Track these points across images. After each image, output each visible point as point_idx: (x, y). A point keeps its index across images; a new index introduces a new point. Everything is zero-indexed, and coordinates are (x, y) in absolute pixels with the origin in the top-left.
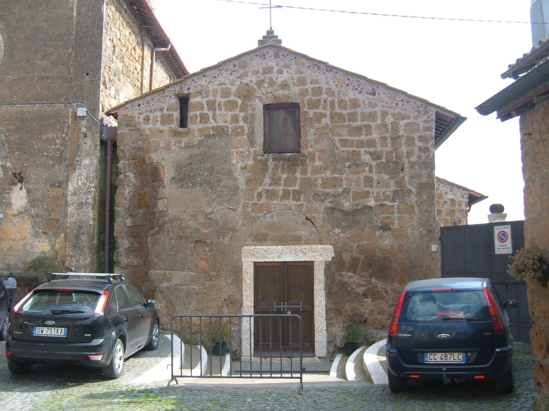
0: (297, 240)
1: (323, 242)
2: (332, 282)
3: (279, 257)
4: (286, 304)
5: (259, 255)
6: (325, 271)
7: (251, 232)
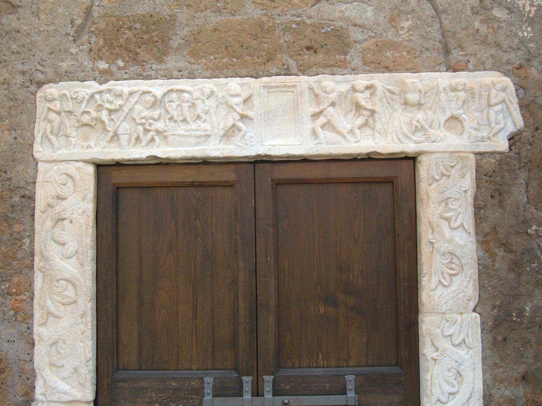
0: (321, 49)
1: (456, 55)
2: (516, 266)
3: (230, 133)
4: (268, 387)
5: (125, 127)
6: (479, 209)
7: (88, 12)
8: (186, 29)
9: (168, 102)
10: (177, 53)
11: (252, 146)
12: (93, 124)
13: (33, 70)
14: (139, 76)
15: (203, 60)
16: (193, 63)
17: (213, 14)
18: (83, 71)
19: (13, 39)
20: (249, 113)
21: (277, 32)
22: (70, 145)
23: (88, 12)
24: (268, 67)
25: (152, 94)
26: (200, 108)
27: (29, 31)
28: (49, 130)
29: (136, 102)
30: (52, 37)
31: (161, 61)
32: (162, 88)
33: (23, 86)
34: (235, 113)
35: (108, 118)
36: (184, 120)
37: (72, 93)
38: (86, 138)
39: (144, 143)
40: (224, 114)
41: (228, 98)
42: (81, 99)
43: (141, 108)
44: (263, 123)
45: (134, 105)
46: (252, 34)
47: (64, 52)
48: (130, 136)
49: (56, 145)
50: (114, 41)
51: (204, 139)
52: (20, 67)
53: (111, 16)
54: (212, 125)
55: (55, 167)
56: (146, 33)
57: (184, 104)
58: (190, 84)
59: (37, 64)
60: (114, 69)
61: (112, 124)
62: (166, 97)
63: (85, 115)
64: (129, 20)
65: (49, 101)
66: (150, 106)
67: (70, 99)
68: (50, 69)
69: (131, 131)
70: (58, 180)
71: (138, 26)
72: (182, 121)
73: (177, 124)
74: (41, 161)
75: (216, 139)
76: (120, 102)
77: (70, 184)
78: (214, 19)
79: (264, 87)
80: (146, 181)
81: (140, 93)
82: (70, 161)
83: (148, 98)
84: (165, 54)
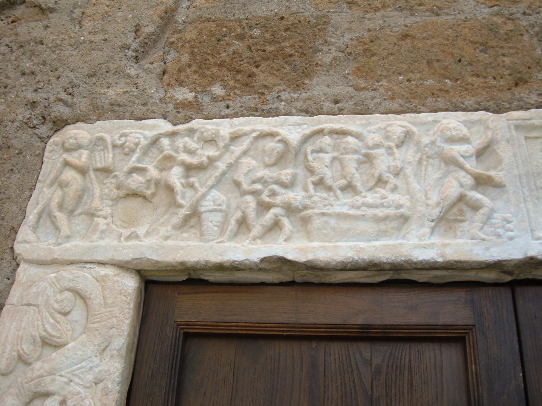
8: (348, 36)
9: (313, 152)
10: (331, 72)
11: (511, 238)
12: (148, 192)
13: (51, 100)
14: (253, 111)
15: (384, 82)
16: (364, 89)
17: (396, 13)
18: (145, 105)
19: (28, 54)
20: (495, 174)
21: (526, 37)
22: (94, 231)
23: (168, 17)
24: (519, 93)
25: (278, 138)
26: (383, 163)
27: (59, 42)
28: (56, 200)
29: (245, 153)
30: (99, 50)
31: (298, 86)
32: (300, 130)
33: (27, 124)
34: (463, 173)
35: (183, 181)
36: (349, 188)
37: (116, 137)
38: (131, 221)
39: (256, 230)
40: (437, 175)
41: (443, 145)
42: (132, 145)
43: (254, 162)
44: (527, 194)
45: (239, 158)
46: (476, 43)
47: (114, 74)
48: (226, 216)
49: (65, 230)
50: (209, 57)
51: (394, 224)
52: (30, 96)
53: (208, 20)
54: (412, 198)
55: (53, 275)
56: (271, 42)
57: (347, 157)
58: (358, 122)
59: (61, 90)
60: (205, 99)
61: (189, 193)
62: (308, 144)
63: (134, 175)
64: (240, 26)
65: (68, 150)
66: (273, 160)
67: (110, 147)
68: (84, 100)
69: (229, 206)
70: (52, 301)
71: (257, 32)
72: (343, 189)
73: (332, 194)
74: (27, 261)
75: (423, 226)
76: (212, 152)
77: (78, 314)
78: (399, 21)
79: (517, 127)
80: (254, 320)
81: (254, 134)
82: (86, 262)
83: (271, 144)
84: (307, 75)
